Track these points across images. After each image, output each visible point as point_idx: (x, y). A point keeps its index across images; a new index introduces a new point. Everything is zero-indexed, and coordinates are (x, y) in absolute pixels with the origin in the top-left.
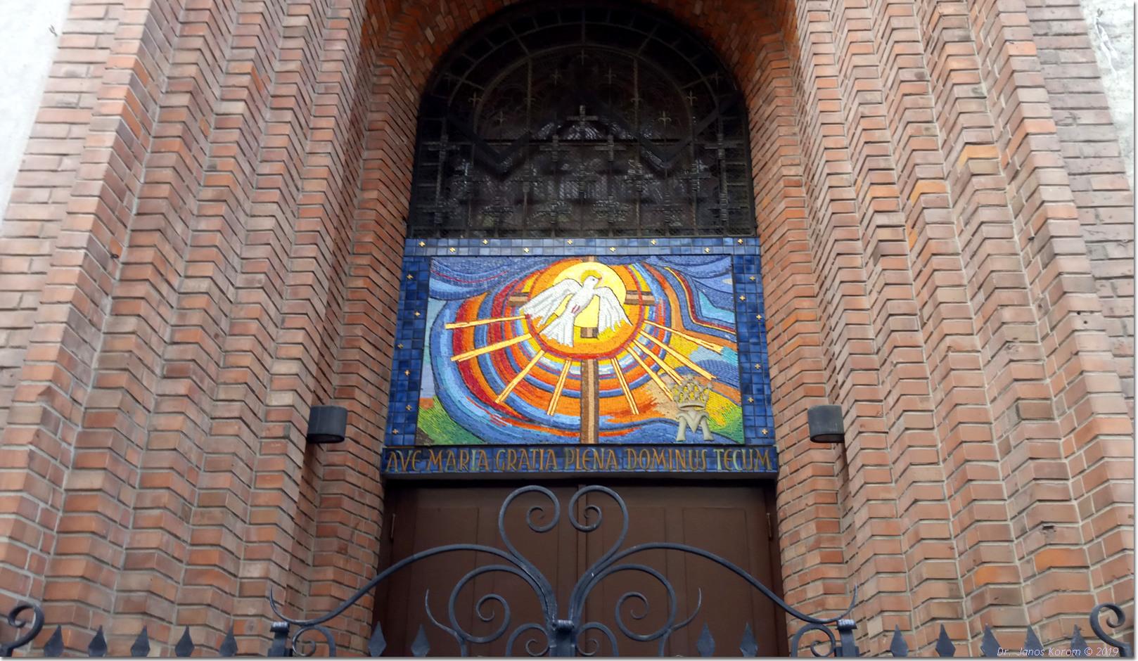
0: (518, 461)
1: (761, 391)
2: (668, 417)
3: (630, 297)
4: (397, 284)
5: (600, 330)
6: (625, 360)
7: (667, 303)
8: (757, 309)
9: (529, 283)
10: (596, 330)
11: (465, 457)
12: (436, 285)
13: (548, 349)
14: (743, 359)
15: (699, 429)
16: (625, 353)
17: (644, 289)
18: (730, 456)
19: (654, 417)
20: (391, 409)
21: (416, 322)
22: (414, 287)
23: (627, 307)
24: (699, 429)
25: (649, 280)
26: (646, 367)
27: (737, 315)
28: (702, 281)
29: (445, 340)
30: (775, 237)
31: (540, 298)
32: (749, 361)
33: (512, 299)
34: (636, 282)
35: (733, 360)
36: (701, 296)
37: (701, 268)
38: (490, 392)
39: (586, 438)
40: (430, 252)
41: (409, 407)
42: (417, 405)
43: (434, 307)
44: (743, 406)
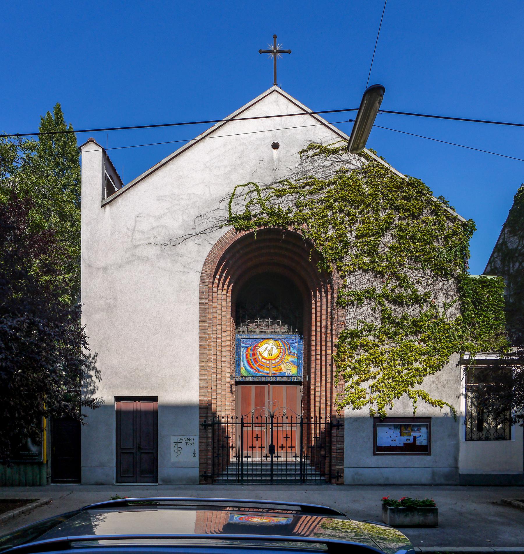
12: (242, 345)
13: (263, 358)
40: (240, 337)
43: (242, 349)
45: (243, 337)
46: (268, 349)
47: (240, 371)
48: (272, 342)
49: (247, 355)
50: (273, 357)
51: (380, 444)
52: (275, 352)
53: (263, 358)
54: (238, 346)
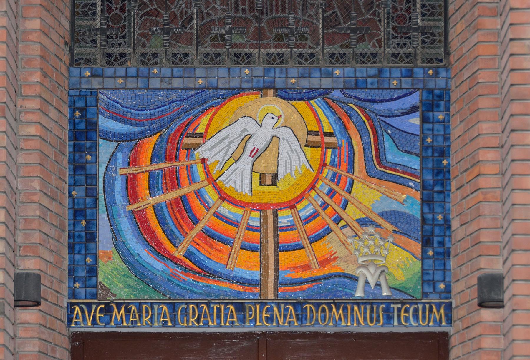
0: (200, 316)
1: (441, 243)
2: (348, 271)
3: (311, 138)
4: (65, 123)
5: (280, 176)
6: (305, 209)
7: (350, 144)
8: (444, 153)
9: (204, 121)
10: (275, 177)
11: (147, 312)
12: (105, 123)
13: (224, 197)
14: (426, 210)
15: (378, 285)
16: (305, 202)
17: (326, 129)
18: (407, 311)
19: (334, 271)
20: (72, 261)
21: (88, 165)
22: (82, 126)
23: (308, 150)
24: (378, 285)
25: (332, 118)
26: (327, 218)
27: (424, 159)
28: (388, 120)
29: (119, 186)
30: (466, 74)
31: (215, 140)
32: (432, 211)
33: (186, 140)
34: (319, 121)
35: (415, 211)
36: (386, 136)
37: (388, 105)
38: (168, 245)
39: (266, 294)
40: (96, 83)
41: (89, 261)
42: (96, 258)
43: (105, 149)
44: (422, 259)
45: (115, 87)
46: (258, 142)
47: (93, 271)
48: (274, 105)
49: (131, 182)
50: (283, 191)
51: (271, 183)
52: (294, 162)
53: (224, 197)
54: (83, 135)
